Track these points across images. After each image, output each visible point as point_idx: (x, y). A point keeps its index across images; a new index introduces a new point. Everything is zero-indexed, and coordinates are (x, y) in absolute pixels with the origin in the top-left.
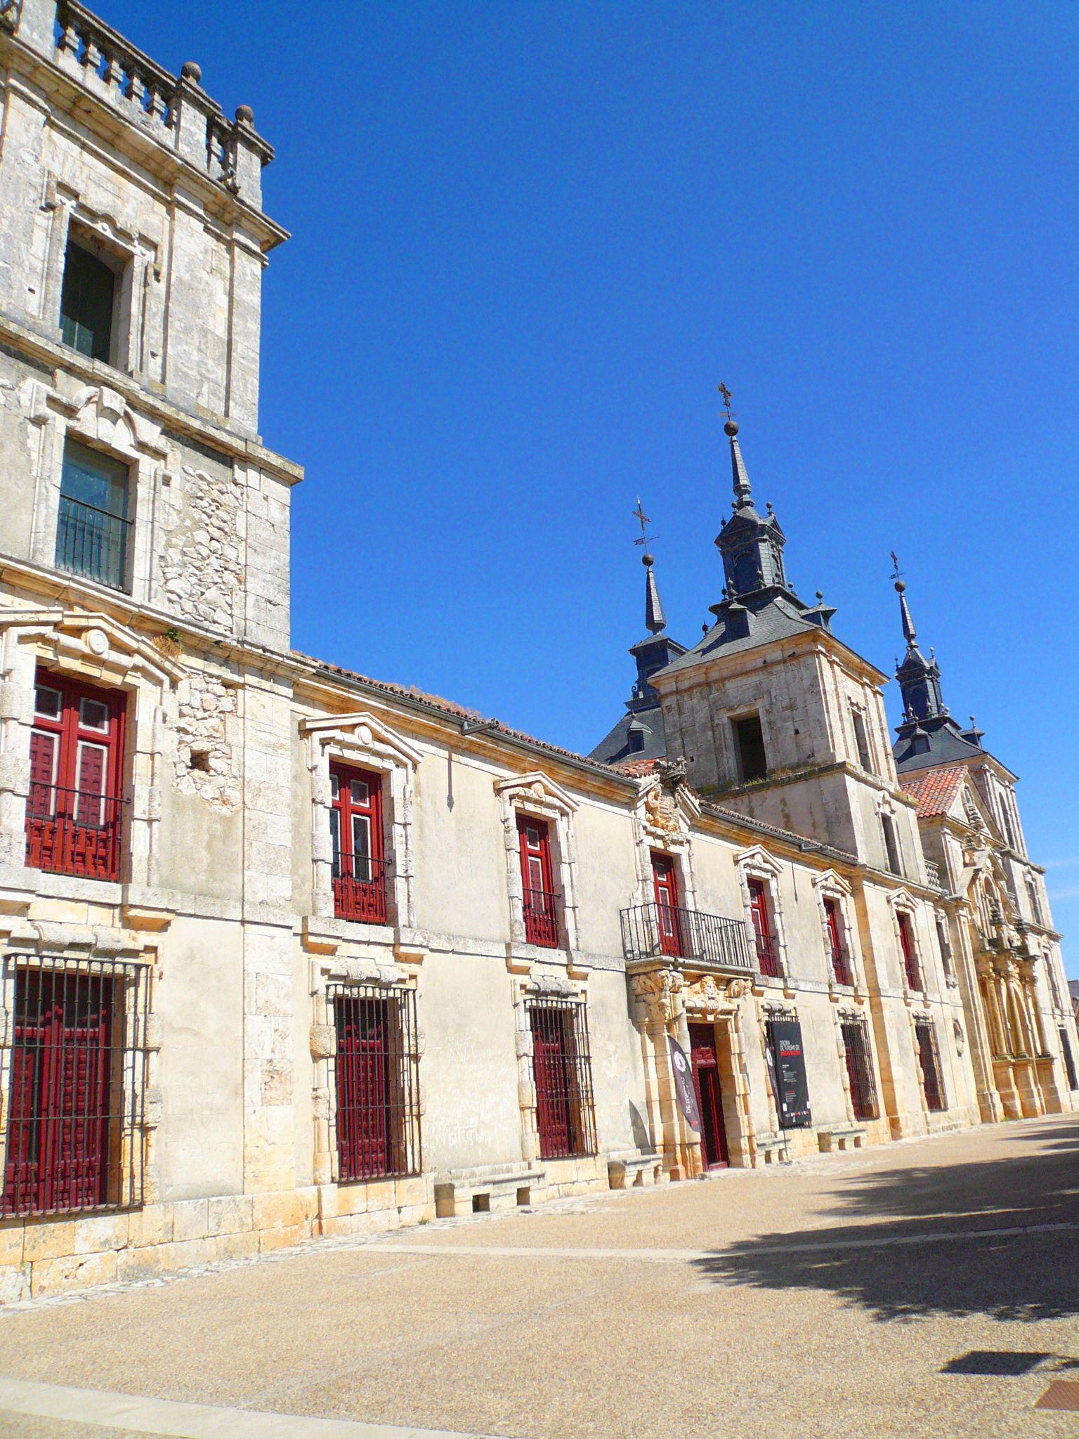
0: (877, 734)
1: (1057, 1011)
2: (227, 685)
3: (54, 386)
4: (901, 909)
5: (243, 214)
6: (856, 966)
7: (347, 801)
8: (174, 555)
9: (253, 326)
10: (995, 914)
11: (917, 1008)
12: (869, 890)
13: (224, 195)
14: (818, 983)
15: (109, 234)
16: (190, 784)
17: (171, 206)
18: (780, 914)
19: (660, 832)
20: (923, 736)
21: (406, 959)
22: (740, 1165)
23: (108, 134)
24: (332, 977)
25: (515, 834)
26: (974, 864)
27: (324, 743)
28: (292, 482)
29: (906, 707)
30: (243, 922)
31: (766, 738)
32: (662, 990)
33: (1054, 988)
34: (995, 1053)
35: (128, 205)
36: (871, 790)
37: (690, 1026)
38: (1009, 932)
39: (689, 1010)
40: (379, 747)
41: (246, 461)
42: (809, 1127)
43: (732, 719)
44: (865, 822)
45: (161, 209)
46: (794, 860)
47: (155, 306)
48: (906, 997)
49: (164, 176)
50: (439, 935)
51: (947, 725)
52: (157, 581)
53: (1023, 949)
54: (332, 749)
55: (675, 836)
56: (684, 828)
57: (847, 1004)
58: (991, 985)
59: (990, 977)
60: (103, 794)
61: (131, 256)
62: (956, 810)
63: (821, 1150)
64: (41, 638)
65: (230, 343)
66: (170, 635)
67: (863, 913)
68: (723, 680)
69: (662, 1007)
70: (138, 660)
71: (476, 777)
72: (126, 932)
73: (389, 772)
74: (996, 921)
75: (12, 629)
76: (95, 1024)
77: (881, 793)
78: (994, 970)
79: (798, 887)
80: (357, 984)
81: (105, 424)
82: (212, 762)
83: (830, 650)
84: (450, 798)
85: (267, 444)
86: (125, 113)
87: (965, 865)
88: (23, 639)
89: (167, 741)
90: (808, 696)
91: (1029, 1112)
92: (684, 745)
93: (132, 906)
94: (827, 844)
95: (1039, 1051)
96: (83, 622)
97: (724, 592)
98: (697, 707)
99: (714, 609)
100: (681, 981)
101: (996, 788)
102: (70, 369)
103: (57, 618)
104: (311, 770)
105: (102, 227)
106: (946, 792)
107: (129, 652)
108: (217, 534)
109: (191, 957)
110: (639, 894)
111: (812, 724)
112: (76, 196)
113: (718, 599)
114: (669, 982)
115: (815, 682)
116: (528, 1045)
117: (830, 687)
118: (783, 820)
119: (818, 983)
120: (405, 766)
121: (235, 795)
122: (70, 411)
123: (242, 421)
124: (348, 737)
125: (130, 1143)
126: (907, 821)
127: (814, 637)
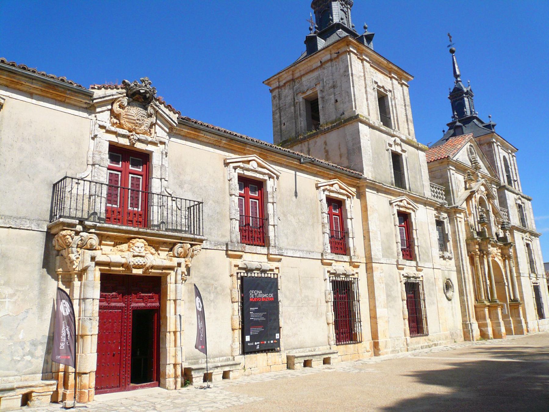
1: (533, 275)
4: (528, 242)
7: (248, 194)
11: (534, 280)
12: (370, 195)
18: (351, 219)
20: (460, 126)
22: (164, 387)
24: (240, 268)
26: (471, 188)
27: (324, 191)
29: (454, 113)
33: (532, 262)
36: (384, 136)
40: (342, 191)
42: (279, 351)
45: (389, 79)
51: (475, 120)
54: (239, 171)
58: (477, 259)
59: (476, 254)
60: (141, 190)
63: (288, 368)
68: (301, 76)
71: (306, 181)
75: (230, 164)
76: (345, 294)
77: (393, 139)
78: (480, 250)
80: (251, 270)
84: (296, 192)
87: (466, 189)
91: (497, 335)
92: (280, 117)
93: (271, 254)
95: (512, 298)
97: (453, 117)
99: (448, 125)
101: (500, 153)
104: (229, 180)
105: (382, 90)
107: (410, 204)
111: (344, 95)
113: (450, 120)
115: (346, 74)
116: (331, 297)
118: (325, 154)
120: (273, 178)
123: (413, 138)
124: (247, 166)
125: (357, 324)
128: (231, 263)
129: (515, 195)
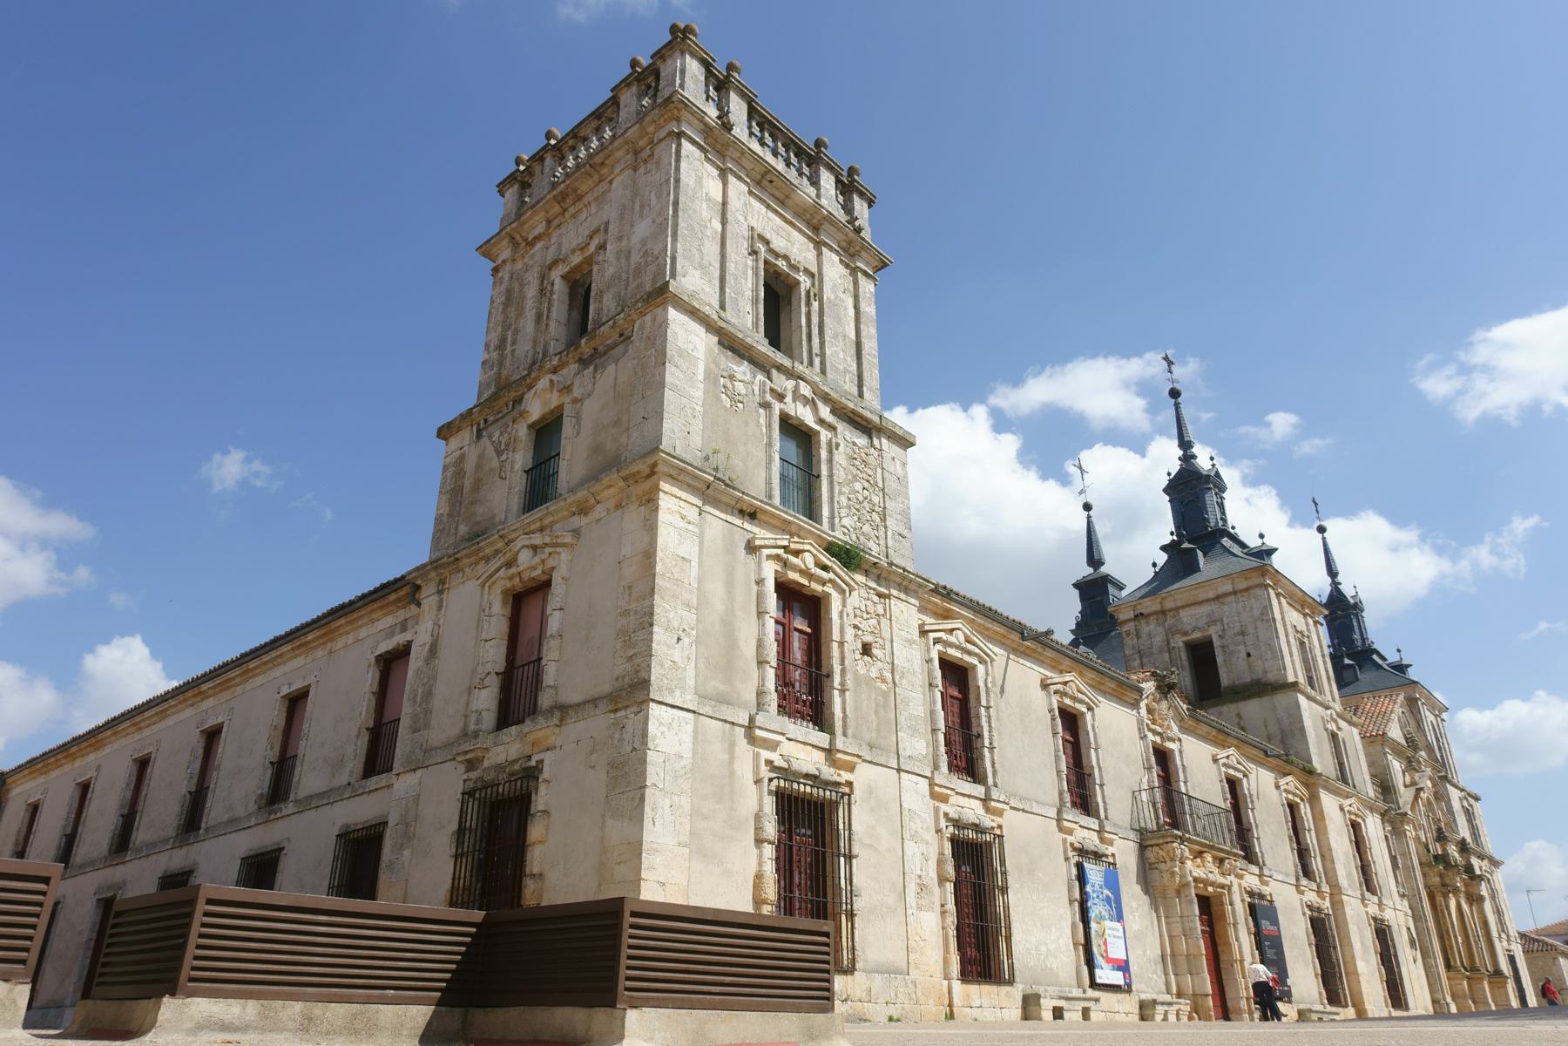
0: (1320, 659)
2: (880, 595)
3: (770, 379)
6: (1316, 864)
9: (870, 332)
10: (1439, 831)
11: (1373, 910)
13: (852, 235)
16: (861, 666)
17: (818, 245)
19: (1159, 729)
27: (937, 641)
30: (899, 770)
31: (1220, 660)
32: (1172, 860)
35: (794, 245)
38: (1453, 850)
39: (1196, 880)
40: (969, 647)
46: (1262, 765)
47: (815, 319)
48: (1363, 899)
51: (1226, 541)
53: (1469, 869)
55: (1170, 734)
56: (1175, 729)
57: (1311, 897)
58: (1439, 899)
61: (798, 283)
62: (1395, 733)
66: (848, 556)
67: (1319, 817)
69: (1173, 874)
70: (831, 575)
74: (1441, 837)
79: (1263, 784)
81: (800, 407)
82: (875, 651)
88: (769, 557)
90: (1259, 623)
94: (1285, 751)
96: (800, 547)
99: (1164, 548)
100: (1187, 854)
102: (780, 368)
103: (785, 543)
105: (781, 264)
106: (1385, 716)
110: (1145, 780)
113: (1168, 539)
114: (1178, 852)
122: (781, 397)
126: (1351, 736)
128: (756, 757)
129: (1320, 708)
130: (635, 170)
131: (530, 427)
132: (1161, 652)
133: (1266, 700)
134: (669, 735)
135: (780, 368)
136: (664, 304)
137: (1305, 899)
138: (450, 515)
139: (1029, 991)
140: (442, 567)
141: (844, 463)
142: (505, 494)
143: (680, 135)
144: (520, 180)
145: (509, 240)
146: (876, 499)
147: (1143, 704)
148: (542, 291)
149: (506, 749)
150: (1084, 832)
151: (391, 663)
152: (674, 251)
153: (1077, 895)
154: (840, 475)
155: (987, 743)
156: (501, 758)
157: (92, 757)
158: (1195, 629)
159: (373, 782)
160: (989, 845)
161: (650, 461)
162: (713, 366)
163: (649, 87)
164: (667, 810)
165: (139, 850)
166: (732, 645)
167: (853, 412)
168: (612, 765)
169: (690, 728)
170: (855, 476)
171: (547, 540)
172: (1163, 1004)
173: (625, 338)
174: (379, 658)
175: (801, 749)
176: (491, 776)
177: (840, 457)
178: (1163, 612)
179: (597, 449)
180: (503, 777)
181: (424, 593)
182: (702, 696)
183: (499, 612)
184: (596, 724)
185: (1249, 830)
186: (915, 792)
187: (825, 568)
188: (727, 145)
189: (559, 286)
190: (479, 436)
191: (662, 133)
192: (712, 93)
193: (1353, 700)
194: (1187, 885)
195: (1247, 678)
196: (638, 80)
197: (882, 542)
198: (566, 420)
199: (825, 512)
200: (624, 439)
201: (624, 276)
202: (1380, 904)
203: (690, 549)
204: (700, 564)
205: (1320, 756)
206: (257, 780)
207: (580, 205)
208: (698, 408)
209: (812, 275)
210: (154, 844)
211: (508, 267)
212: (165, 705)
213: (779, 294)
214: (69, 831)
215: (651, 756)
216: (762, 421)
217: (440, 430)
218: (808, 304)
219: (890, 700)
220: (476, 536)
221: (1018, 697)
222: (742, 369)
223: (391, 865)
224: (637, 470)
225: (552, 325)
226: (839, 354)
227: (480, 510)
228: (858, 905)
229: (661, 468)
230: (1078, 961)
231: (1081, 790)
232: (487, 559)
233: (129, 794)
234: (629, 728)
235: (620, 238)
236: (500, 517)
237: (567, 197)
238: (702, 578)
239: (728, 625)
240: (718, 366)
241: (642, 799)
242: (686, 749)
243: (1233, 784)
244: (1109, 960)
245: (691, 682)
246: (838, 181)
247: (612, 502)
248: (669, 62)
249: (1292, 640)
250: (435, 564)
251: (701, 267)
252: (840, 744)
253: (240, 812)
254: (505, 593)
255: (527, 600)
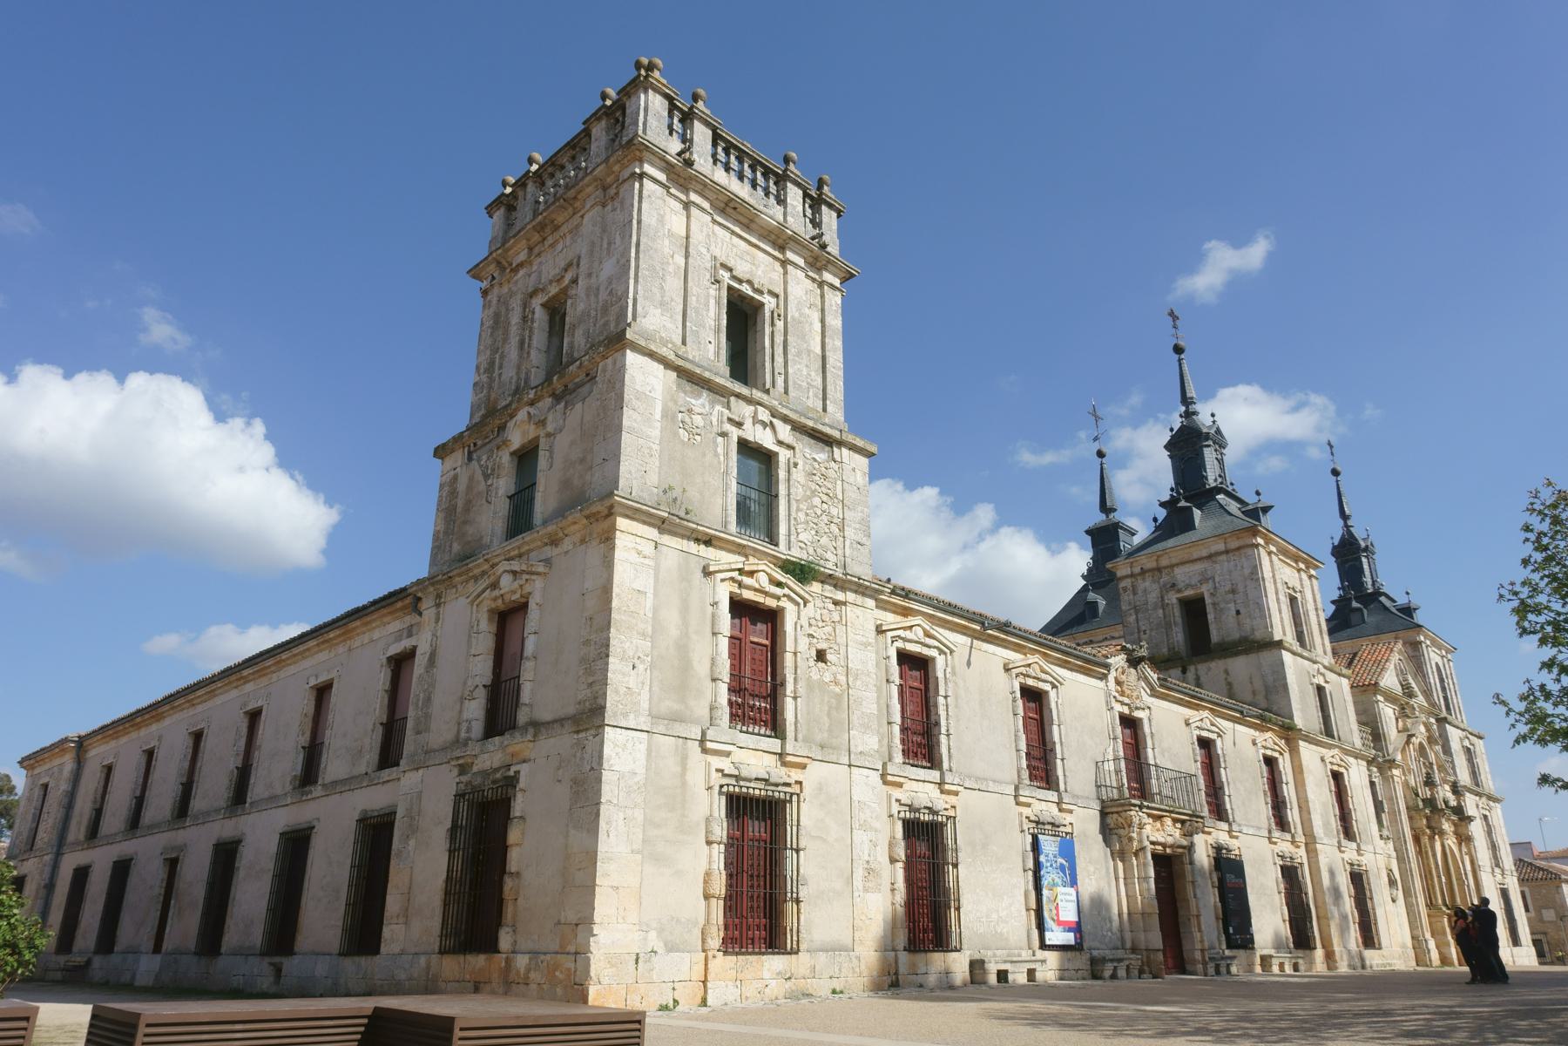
1: (1497, 870)
3: (729, 408)
5: (829, 261)
6: (1293, 815)
8: (801, 516)
9: (836, 344)
14: (1259, 828)
15: (750, 292)
16: (816, 672)
19: (1126, 700)
21: (949, 793)
23: (745, 221)
25: (1020, 703)
28: (869, 455)
31: (1211, 617)
33: (1494, 847)
34: (1431, 905)
35: (758, 267)
37: (1154, 856)
39: (1153, 843)
40: (1044, 676)
41: (840, 443)
43: (1180, 600)
44: (1301, 692)
45: (777, 265)
47: (779, 339)
48: (1340, 846)
49: (779, 240)
50: (970, 777)
52: (797, 541)
53: (1459, 811)
54: (900, 644)
57: (1285, 847)
58: (1425, 840)
61: (763, 304)
64: (732, 579)
65: (824, 358)
66: (802, 572)
67: (1298, 770)
69: (1131, 839)
72: (784, 770)
73: (933, 659)
74: (1429, 782)
79: (1242, 745)
80: (918, 810)
82: (829, 657)
83: (1268, 541)
85: (851, 431)
86: (752, 202)
89: (804, 643)
94: (1267, 707)
98: (1150, 589)
99: (1163, 505)
101: (1433, 657)
102: (738, 396)
105: (746, 289)
108: (825, 498)
109: (820, 789)
110: (1110, 750)
112: (731, 270)
113: (1166, 497)
114: (1136, 820)
115: (1254, 576)
117: (1267, 574)
119: (1259, 828)
121: (842, 679)
122: (739, 425)
123: (834, 418)
124: (908, 634)
125: (790, 907)
126: (1340, 687)
127: (1254, 532)
128: (889, 797)
130: (604, 206)
131: (512, 454)
132: (1155, 609)
133: (1252, 658)
134: (623, 754)
135: (738, 396)
136: (623, 348)
137: (1277, 849)
138: (446, 533)
139: (977, 956)
140: (439, 583)
141: (802, 480)
142: (491, 518)
143: (642, 176)
144: (505, 204)
145: (493, 269)
146: (834, 511)
147: (1111, 678)
148: (524, 319)
149: (490, 757)
150: (1043, 804)
151: (400, 664)
152: (636, 292)
153: (1030, 864)
154: (797, 492)
155: (943, 730)
156: (487, 766)
157: (154, 727)
158: (1188, 586)
159: (386, 774)
160: (942, 825)
161: (607, 503)
162: (670, 404)
163: (617, 121)
164: (621, 822)
165: (196, 817)
166: (685, 667)
167: (813, 429)
168: (575, 782)
169: (643, 747)
170: (813, 492)
171: (524, 567)
172: (1112, 961)
173: (591, 378)
174: (390, 659)
175: (753, 757)
176: (478, 781)
177: (798, 475)
178: (1159, 569)
179: (566, 484)
180: (488, 784)
181: (424, 605)
182: (655, 717)
183: (486, 628)
184: (558, 743)
185: (1222, 788)
186: (866, 785)
187: (779, 584)
188: (691, 178)
189: (540, 315)
190: (470, 459)
191: (626, 174)
192: (677, 125)
193: (1347, 646)
194: (1143, 849)
195: (1236, 635)
196: (606, 114)
197: (840, 552)
198: (541, 453)
199: (783, 529)
200: (588, 477)
201: (593, 313)
202: (1359, 850)
203: (645, 582)
204: (655, 595)
205: (1303, 710)
206: (293, 763)
207: (557, 235)
208: (655, 447)
209: (777, 296)
210: (208, 813)
211: (496, 290)
212: (213, 686)
213: (743, 317)
214: (138, 793)
215: (606, 776)
216: (720, 450)
217: (436, 450)
218: (773, 324)
219: (842, 702)
220: (465, 557)
221: (979, 686)
222: (701, 402)
223: (400, 852)
224: (596, 509)
225: (533, 353)
226: (803, 371)
227: (470, 530)
228: (803, 893)
229: (617, 509)
230: (1029, 924)
231: (1042, 765)
232: (476, 578)
233: (186, 765)
234: (589, 749)
235: (590, 275)
236: (487, 540)
237: (546, 228)
238: (658, 603)
239: (683, 648)
240: (676, 402)
241: (598, 815)
242: (640, 765)
243: (1205, 744)
244: (1060, 923)
245: (645, 705)
246: (806, 195)
247: (578, 537)
248: (633, 99)
249: (1282, 598)
250: (431, 580)
251: (662, 304)
252: (789, 749)
253: (279, 791)
254: (491, 611)
255: (509, 618)
